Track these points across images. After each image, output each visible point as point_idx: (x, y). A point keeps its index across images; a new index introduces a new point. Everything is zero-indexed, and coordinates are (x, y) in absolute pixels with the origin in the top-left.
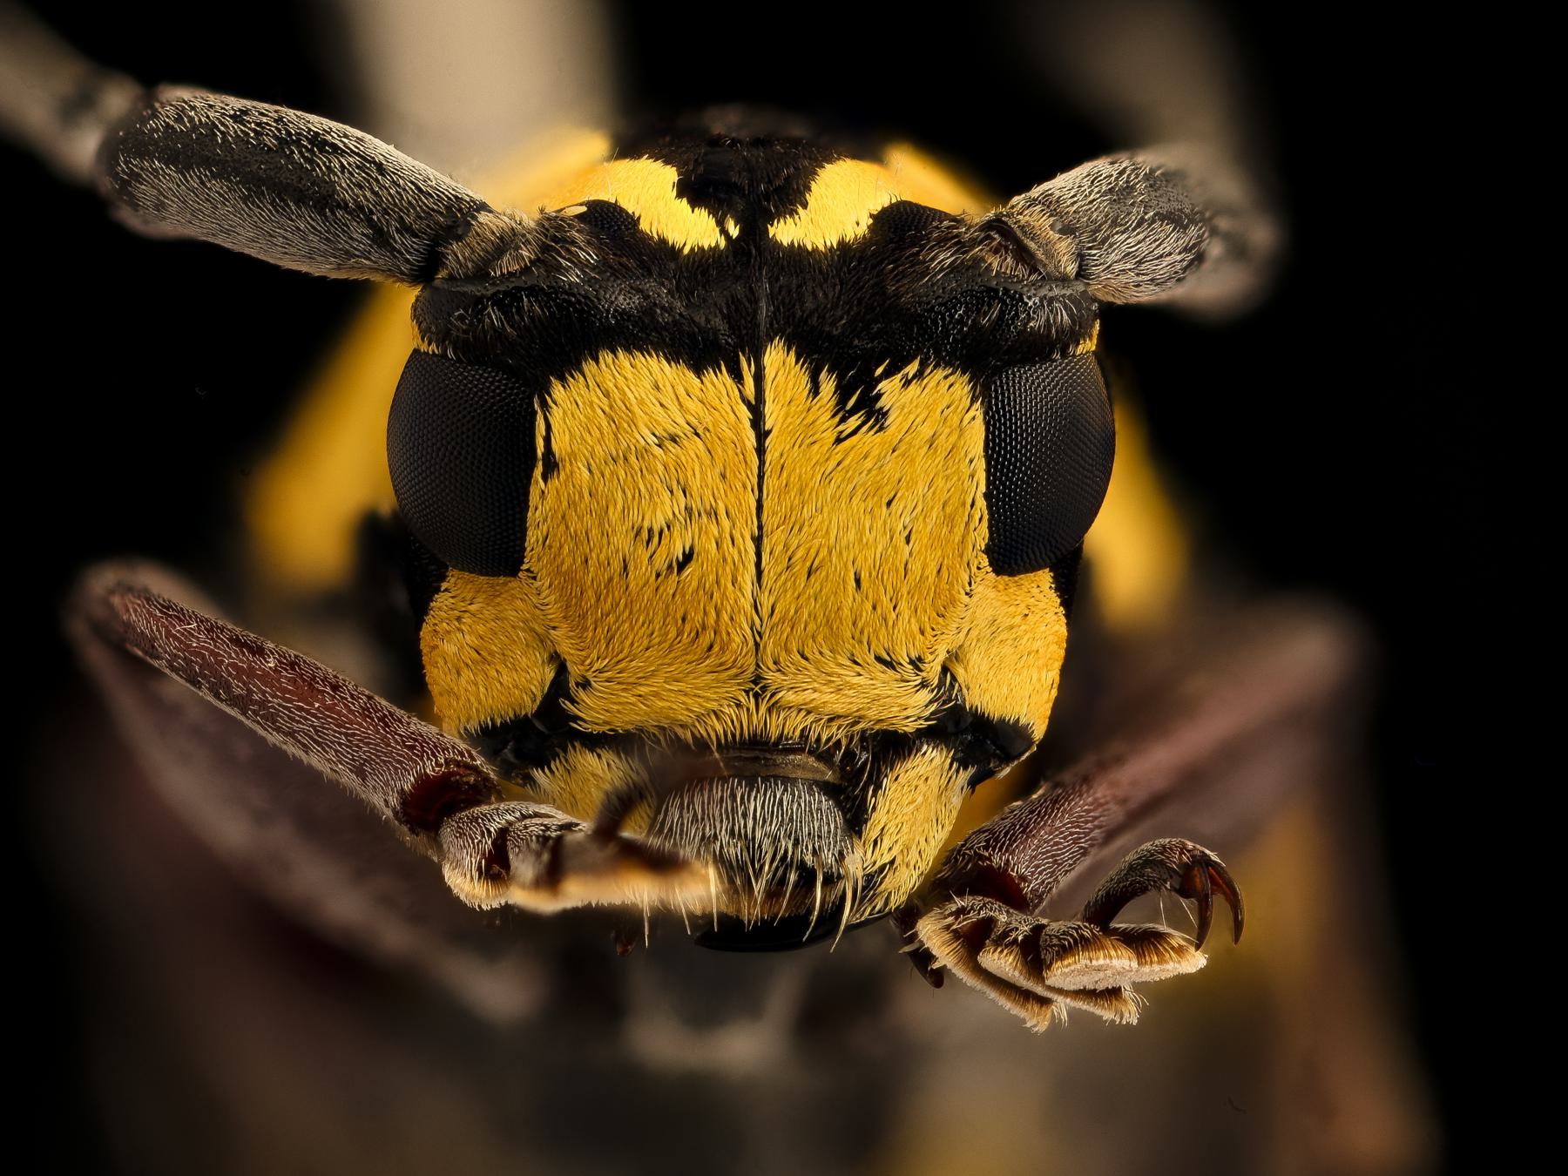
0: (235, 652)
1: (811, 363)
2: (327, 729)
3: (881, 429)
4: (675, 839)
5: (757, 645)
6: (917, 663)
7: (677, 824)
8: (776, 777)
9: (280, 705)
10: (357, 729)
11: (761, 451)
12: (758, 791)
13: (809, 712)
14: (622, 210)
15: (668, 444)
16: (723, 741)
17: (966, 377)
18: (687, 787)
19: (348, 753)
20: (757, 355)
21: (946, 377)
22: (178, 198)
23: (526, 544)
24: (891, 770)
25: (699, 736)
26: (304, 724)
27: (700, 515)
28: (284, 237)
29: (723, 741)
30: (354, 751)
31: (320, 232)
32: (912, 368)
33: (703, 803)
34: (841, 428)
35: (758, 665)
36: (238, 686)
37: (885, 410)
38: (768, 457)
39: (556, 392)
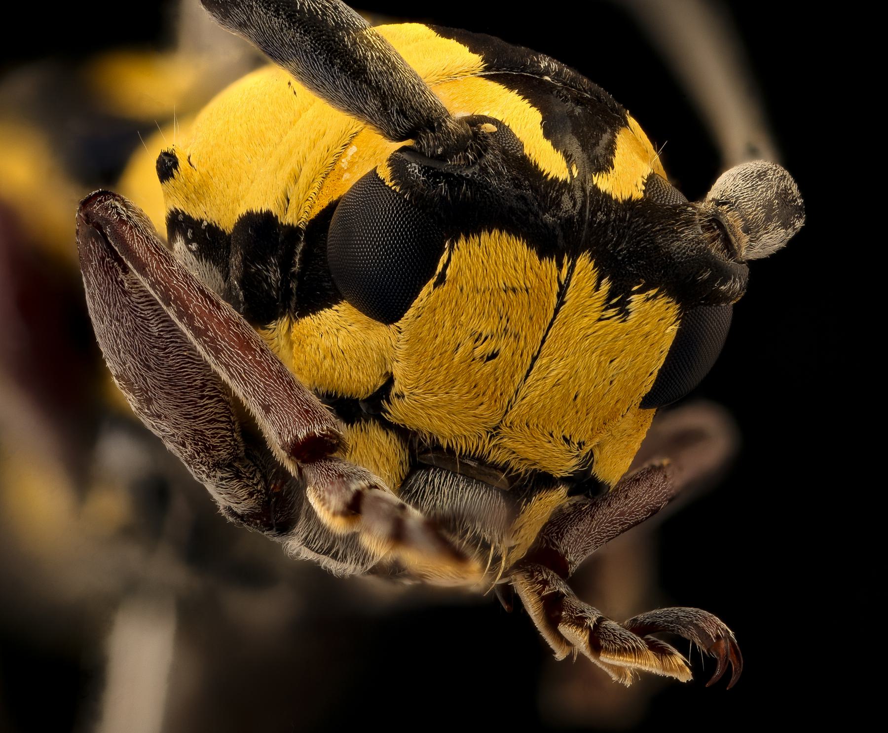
0: (201, 299)
1: (600, 272)
2: (253, 374)
3: (624, 321)
4: (418, 499)
5: (507, 411)
6: (581, 444)
7: (421, 490)
8: (485, 483)
9: (226, 347)
10: (272, 383)
11: (557, 311)
12: (472, 488)
13: (514, 453)
14: (511, 131)
15: (511, 294)
16: (463, 454)
17: (678, 306)
18: (432, 471)
19: (262, 394)
20: (574, 257)
21: (668, 303)
22: (260, 28)
23: (405, 314)
24: (539, 493)
25: (451, 446)
26: (238, 364)
27: (511, 336)
28: (322, 82)
29: (463, 454)
30: (266, 395)
31: (348, 91)
32: (652, 292)
33: (440, 483)
34: (603, 313)
35: (501, 421)
36: (199, 321)
37: (629, 311)
38: (559, 316)
39: (461, 242)
